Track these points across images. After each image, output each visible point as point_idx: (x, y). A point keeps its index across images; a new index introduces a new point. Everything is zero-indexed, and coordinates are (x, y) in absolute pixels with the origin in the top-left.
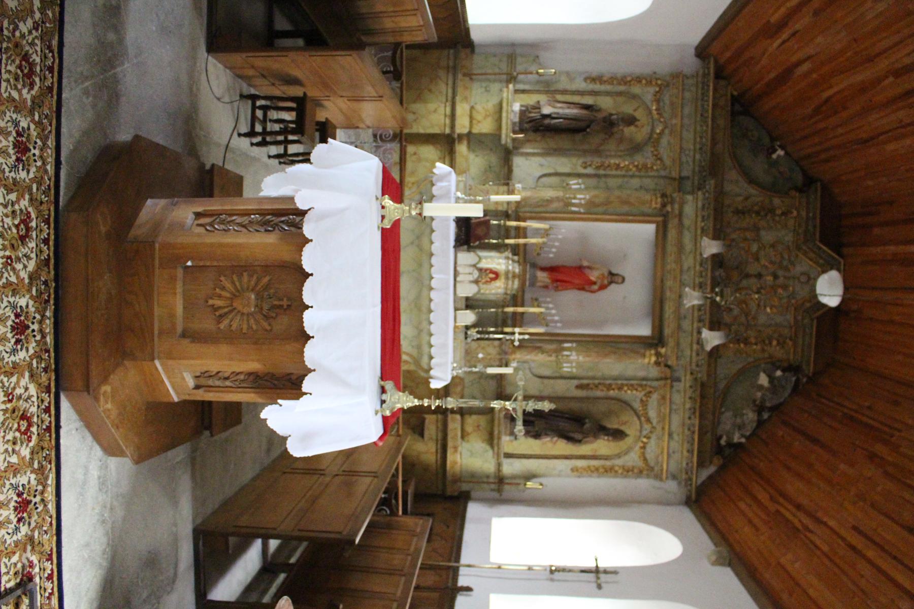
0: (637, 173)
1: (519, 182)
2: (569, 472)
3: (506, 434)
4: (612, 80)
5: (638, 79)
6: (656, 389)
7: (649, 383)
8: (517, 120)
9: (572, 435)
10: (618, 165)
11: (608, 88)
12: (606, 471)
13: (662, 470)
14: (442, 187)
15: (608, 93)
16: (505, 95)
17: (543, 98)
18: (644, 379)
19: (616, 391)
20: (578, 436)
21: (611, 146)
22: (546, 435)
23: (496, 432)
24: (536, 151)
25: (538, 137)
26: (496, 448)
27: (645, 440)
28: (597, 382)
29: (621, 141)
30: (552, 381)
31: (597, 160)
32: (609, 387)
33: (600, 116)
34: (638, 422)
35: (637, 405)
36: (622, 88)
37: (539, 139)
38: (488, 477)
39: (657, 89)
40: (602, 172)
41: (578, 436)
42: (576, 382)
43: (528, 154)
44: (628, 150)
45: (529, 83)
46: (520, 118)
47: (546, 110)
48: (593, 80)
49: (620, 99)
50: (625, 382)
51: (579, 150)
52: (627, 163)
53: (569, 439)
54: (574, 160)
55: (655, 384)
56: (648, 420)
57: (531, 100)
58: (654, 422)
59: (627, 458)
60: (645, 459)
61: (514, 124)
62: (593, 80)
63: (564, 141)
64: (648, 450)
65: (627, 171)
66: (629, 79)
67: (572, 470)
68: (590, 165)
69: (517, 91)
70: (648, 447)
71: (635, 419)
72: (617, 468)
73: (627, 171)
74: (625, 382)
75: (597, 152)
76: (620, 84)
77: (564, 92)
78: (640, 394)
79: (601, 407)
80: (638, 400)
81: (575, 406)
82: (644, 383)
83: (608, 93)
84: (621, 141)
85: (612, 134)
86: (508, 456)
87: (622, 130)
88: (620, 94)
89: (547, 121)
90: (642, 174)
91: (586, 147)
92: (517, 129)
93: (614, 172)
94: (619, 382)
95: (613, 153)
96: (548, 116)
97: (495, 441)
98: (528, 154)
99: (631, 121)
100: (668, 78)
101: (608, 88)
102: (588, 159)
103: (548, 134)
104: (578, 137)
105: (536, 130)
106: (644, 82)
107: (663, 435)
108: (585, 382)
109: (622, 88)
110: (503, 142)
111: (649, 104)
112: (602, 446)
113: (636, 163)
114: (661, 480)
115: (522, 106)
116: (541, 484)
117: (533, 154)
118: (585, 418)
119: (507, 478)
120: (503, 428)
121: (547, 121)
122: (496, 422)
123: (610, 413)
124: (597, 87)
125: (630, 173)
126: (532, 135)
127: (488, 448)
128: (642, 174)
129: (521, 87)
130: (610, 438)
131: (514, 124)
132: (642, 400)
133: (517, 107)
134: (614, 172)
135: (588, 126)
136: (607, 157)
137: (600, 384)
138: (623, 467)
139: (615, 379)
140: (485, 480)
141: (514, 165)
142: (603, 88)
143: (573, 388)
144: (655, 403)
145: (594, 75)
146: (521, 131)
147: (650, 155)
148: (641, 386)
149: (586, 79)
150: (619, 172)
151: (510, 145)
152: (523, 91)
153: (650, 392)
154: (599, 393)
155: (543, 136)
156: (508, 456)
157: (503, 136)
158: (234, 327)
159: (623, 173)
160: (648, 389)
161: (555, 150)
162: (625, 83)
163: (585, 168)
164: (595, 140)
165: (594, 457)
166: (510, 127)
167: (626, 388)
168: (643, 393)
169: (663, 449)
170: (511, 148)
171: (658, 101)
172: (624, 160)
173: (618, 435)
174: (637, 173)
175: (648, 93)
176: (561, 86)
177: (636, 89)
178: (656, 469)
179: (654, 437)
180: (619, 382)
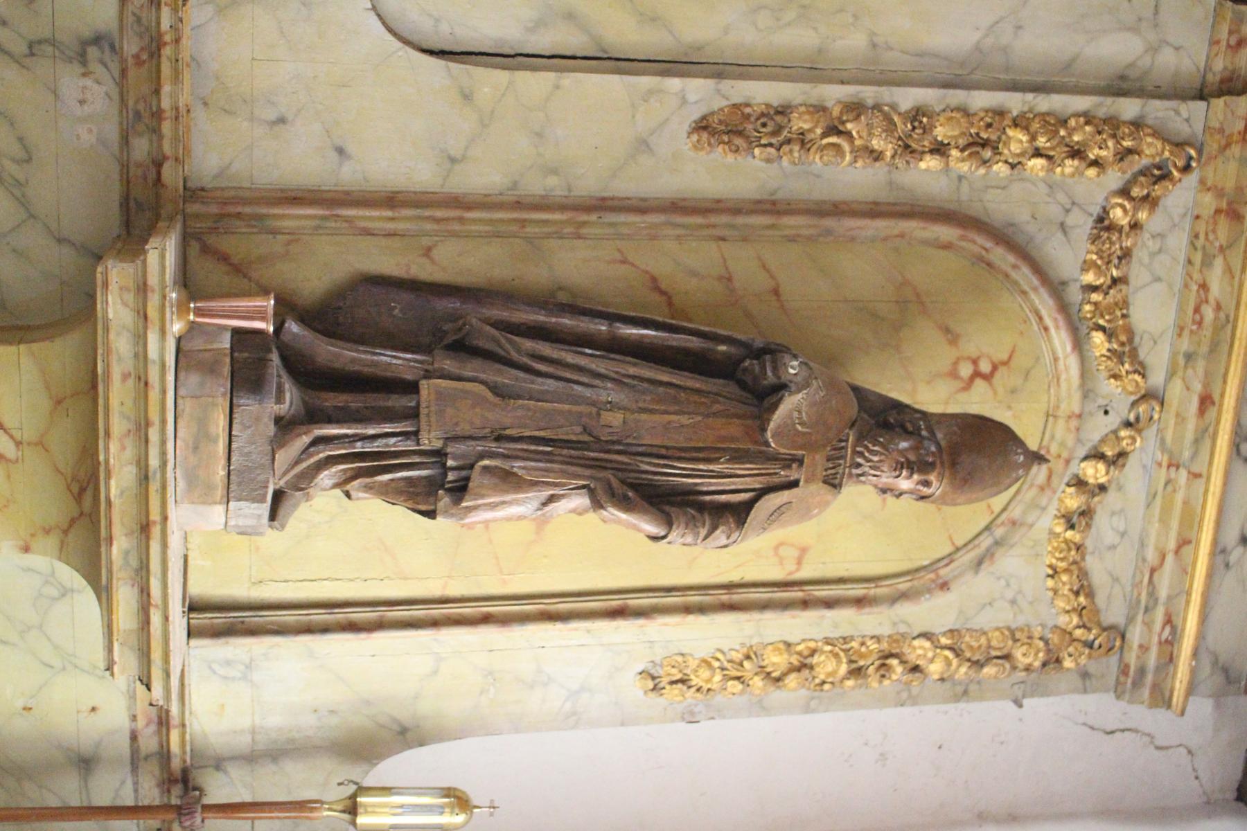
2: (633, 690)
3: (199, 491)
6: (1187, 152)
7: (1157, 110)
9: (678, 475)
12: (857, 673)
13: (1169, 645)
18: (1120, 86)
19: (960, 164)
20: (726, 480)
22: (510, 481)
23: (119, 484)
26: (125, 597)
27: (1094, 472)
28: (833, 94)
30: (534, 83)
32: (914, 138)
34: (1070, 365)
35: (1070, 256)
38: (85, 763)
39: (163, 255)
41: (726, 480)
42: (700, 94)
50: (1015, 102)
53: (668, 503)
55: (1190, 117)
56: (1127, 352)
58: (1158, 359)
59: (979, 586)
60: (1084, 588)
64: (1105, 526)
67: (654, 682)
70: (1105, 506)
71: (1061, 340)
72: (919, 650)
74: (1015, 102)
78: (1096, 187)
79: (865, 264)
80: (1083, 224)
81: (686, 264)
82: (1129, 108)
86: (221, 619)
94: (981, 100)
97: (120, 547)
107: (1205, 434)
108: (763, 93)
112: (857, 523)
114: (1161, 698)
116: (460, 800)
118: (771, 352)
119: (219, 764)
120: (173, 448)
122: (118, 395)
123: (902, 312)
127: (70, 576)
130: (937, 487)
132: (1103, 224)
137: (856, 109)
138: (955, 644)
139: (956, 79)
140: (69, 791)
143: (676, 137)
144: (1179, 242)
148: (1111, 125)
153: (1159, 174)
154: (848, 176)
156: (221, 619)
158: (1111, 566)
160: (1152, 150)
165: (794, 594)
167: (1017, 140)
168: (1114, 178)
169: (1190, 519)
173: (972, 451)
178: (1136, 635)
179: (1144, 450)
180: (981, 100)
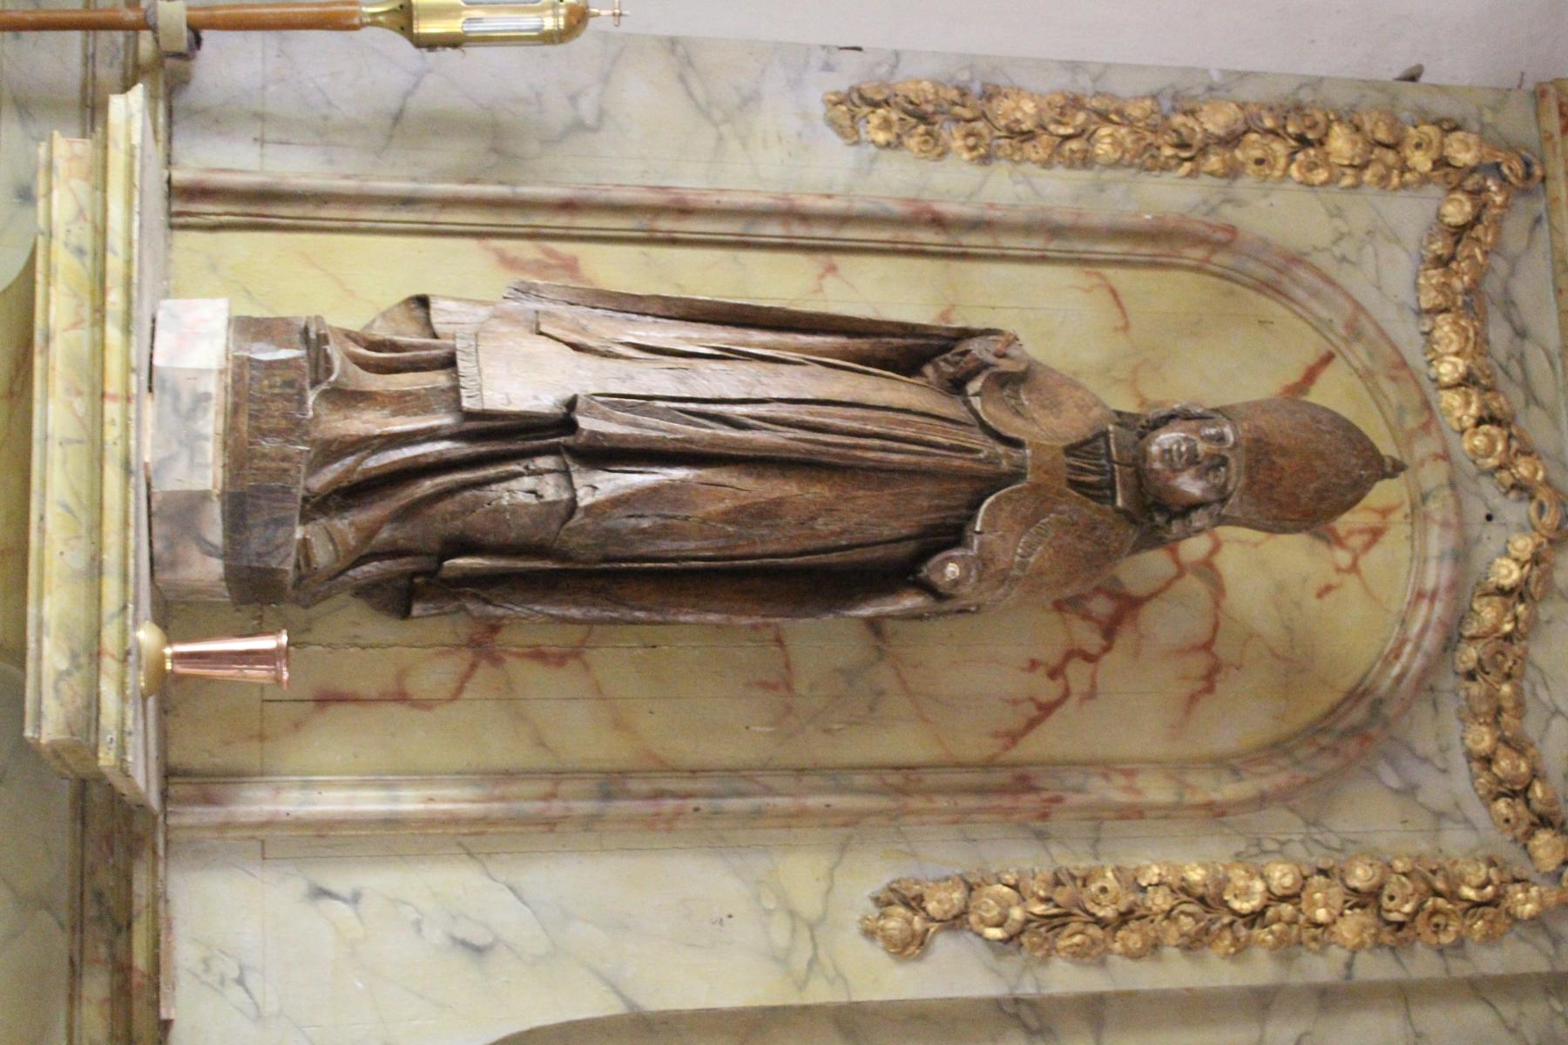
0: (1376, 968)
1: (1518, 767)
4: (1070, 125)
5: (1299, 127)
8: (203, 472)
10: (1208, 901)
11: (1052, 189)
14: (450, 568)
15: (1054, 240)
16: (63, 203)
17: (463, 281)
21: (1125, 717)
24: (410, 801)
25: (423, 647)
29: (1209, 666)
31: (1017, 864)
33: (1045, 428)
36: (1170, 195)
37: (434, 675)
39: (1457, 210)
40: (1065, 978)
43: (325, 838)
44: (1277, 749)
45: (323, 131)
46: (238, 457)
47: (518, 376)
48: (920, 118)
49: (1159, 293)
51: (837, 776)
52: (1282, 876)
54: (801, 872)
57: (350, 284)
61: (170, 517)
62: (920, 118)
63: (683, 688)
65: (1286, 949)
66: (1216, 121)
68: (956, 922)
69: (190, 203)
73: (1286, 949)
75: (1013, 788)
76: (1146, 160)
77: (662, 220)
83: (1054, 240)
84: (1209, 666)
85: (1129, 605)
87: (1207, 568)
88: (1158, 242)
89: (527, 489)
90: (1423, 964)
91: (903, 743)
92: (206, 570)
93: (1177, 972)
95: (1157, 791)
96: (550, 434)
98: (325, 838)
99: (1307, 479)
100: (1517, 122)
101: (1052, 189)
102: (938, 859)
103: (530, 621)
104: (823, 640)
105: (412, 584)
106: (1341, 143)
109: (1170, 195)
110: (49, 722)
111: (1406, 333)
113: (1361, 876)
115: (249, 328)
117: (391, 838)
121: (527, 489)
124: (954, 181)
125: (1322, 968)
126: (366, 645)
128: (1423, 964)
129: (208, 158)
131: (170, 517)
133: (197, 339)
134: (1177, 972)
135: (949, 535)
136: (1105, 821)
141: (184, 954)
142: (1007, 187)
145: (919, 77)
146: (256, 590)
147: (1461, 784)
149: (852, 108)
150: (1217, 972)
151: (129, 754)
152: (261, 207)
155: (483, 646)
157: (51, 656)
159: (1261, 970)
161: (610, 784)
162: (1190, 150)
163: (911, 947)
164: (975, 664)
166: (124, 543)
170: (143, 780)
171: (1471, 305)
172: (1254, 857)
174: (1376, 968)
175: (1380, 243)
176: (625, 167)
177: (1281, 208)
